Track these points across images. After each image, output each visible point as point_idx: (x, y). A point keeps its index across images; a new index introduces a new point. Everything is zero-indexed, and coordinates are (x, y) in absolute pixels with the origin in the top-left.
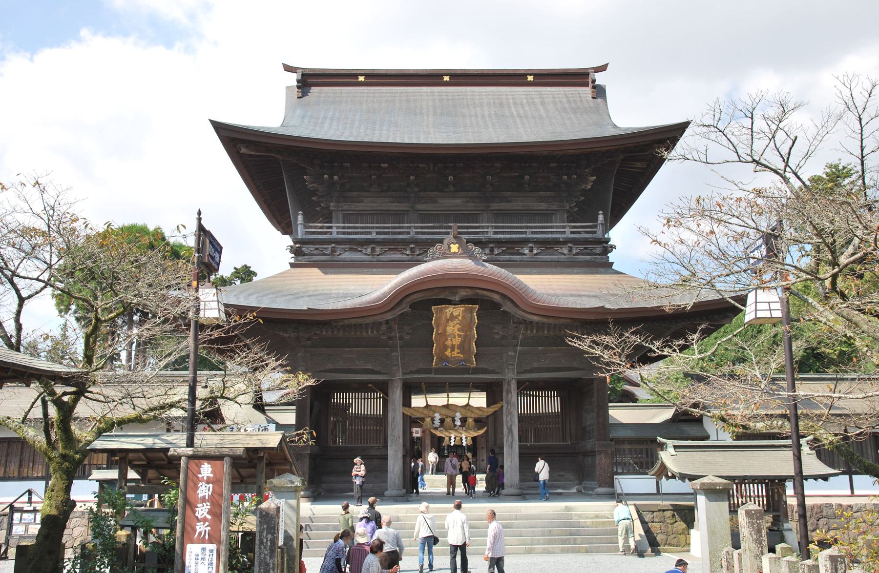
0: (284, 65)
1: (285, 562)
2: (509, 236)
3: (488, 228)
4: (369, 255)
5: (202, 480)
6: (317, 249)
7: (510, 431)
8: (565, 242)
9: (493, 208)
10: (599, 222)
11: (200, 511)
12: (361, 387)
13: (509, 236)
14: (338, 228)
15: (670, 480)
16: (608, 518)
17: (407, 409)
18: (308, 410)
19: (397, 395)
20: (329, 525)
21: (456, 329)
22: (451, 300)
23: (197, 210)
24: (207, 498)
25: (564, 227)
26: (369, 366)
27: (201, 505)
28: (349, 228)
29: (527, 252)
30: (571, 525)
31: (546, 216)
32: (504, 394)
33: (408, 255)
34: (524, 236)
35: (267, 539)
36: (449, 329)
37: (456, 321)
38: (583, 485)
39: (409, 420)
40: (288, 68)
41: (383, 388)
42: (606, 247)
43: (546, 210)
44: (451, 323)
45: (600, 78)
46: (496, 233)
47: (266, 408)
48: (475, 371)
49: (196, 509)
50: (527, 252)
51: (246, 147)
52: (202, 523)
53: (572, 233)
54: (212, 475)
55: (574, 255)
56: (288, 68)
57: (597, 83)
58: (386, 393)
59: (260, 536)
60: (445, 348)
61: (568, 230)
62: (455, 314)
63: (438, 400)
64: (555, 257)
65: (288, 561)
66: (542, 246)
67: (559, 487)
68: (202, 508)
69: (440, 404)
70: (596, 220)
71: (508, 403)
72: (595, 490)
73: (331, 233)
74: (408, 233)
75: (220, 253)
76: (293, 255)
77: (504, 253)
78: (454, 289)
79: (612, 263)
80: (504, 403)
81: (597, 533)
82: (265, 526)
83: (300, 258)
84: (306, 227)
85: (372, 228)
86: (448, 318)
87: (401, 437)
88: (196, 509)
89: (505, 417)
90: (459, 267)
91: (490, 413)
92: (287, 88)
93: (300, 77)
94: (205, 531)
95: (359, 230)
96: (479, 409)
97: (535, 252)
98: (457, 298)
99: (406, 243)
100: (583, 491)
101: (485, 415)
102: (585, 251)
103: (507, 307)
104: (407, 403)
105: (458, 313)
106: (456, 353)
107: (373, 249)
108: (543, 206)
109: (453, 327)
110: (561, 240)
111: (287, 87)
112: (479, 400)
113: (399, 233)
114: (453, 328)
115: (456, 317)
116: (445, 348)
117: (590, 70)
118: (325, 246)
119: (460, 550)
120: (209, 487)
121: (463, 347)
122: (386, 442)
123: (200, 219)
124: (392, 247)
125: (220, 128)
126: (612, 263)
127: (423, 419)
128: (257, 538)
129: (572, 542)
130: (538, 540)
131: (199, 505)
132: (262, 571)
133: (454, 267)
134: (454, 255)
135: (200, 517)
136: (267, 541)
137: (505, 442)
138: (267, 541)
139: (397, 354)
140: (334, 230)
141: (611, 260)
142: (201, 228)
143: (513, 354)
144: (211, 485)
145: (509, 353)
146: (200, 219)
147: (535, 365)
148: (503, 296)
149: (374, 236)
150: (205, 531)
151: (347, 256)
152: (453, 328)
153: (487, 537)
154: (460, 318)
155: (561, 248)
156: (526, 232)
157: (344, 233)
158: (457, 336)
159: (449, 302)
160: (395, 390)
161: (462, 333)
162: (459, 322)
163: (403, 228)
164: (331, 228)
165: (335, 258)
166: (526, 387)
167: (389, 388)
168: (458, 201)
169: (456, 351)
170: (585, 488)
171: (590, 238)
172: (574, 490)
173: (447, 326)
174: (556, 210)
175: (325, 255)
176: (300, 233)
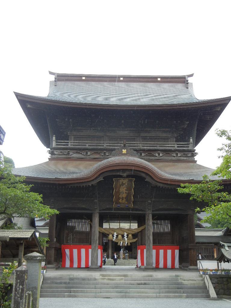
0: (49, 71)
1: (31, 302)
4: (85, 155)
6: (61, 152)
8: (175, 151)
9: (141, 136)
10: (190, 142)
12: (79, 217)
14: (71, 143)
16: (196, 281)
17: (101, 228)
18: (55, 227)
19: (96, 220)
20: (62, 282)
21: (124, 189)
26: (84, 206)
29: (157, 155)
30: (178, 284)
31: (166, 139)
32: (146, 221)
34: (156, 148)
35: (19, 288)
36: (121, 190)
37: (124, 186)
38: (182, 265)
40: (51, 73)
41: (89, 217)
42: (193, 153)
45: (190, 80)
47: (37, 228)
48: (133, 210)
50: (157, 155)
51: (30, 105)
53: (178, 147)
55: (179, 157)
56: (51, 73)
58: (91, 221)
59: (16, 286)
60: (119, 198)
61: (176, 146)
62: (124, 182)
63: (114, 225)
64: (170, 158)
65: (32, 301)
69: (116, 228)
70: (189, 141)
71: (148, 225)
73: (68, 145)
74: (103, 146)
75: (4, 135)
76: (50, 155)
77: (146, 155)
78: (124, 171)
79: (196, 161)
80: (146, 226)
81: (191, 288)
82: (19, 281)
83: (53, 156)
84: (56, 142)
85: (87, 143)
86: (121, 184)
87: (98, 240)
89: (146, 231)
92: (50, 82)
93: (56, 77)
96: (135, 229)
98: (125, 175)
99: (102, 150)
100: (182, 268)
101: (136, 231)
102: (183, 155)
103: (148, 179)
104: (101, 225)
107: (87, 153)
108: (164, 135)
115: (124, 184)
116: (119, 198)
118: (65, 151)
119: (2, 273)
121: (128, 198)
126: (196, 161)
127: (108, 235)
128: (14, 288)
129: (179, 292)
132: (16, 306)
134: (124, 154)
138: (19, 290)
140: (70, 143)
141: (196, 160)
145: (149, 201)
147: (161, 207)
149: (87, 147)
154: (126, 184)
157: (74, 145)
159: (121, 176)
160: (95, 218)
164: (68, 143)
165: (69, 156)
166: (157, 218)
167: (93, 216)
168: (126, 132)
169: (124, 200)
170: (183, 266)
173: (120, 188)
175: (65, 155)
176: (54, 144)
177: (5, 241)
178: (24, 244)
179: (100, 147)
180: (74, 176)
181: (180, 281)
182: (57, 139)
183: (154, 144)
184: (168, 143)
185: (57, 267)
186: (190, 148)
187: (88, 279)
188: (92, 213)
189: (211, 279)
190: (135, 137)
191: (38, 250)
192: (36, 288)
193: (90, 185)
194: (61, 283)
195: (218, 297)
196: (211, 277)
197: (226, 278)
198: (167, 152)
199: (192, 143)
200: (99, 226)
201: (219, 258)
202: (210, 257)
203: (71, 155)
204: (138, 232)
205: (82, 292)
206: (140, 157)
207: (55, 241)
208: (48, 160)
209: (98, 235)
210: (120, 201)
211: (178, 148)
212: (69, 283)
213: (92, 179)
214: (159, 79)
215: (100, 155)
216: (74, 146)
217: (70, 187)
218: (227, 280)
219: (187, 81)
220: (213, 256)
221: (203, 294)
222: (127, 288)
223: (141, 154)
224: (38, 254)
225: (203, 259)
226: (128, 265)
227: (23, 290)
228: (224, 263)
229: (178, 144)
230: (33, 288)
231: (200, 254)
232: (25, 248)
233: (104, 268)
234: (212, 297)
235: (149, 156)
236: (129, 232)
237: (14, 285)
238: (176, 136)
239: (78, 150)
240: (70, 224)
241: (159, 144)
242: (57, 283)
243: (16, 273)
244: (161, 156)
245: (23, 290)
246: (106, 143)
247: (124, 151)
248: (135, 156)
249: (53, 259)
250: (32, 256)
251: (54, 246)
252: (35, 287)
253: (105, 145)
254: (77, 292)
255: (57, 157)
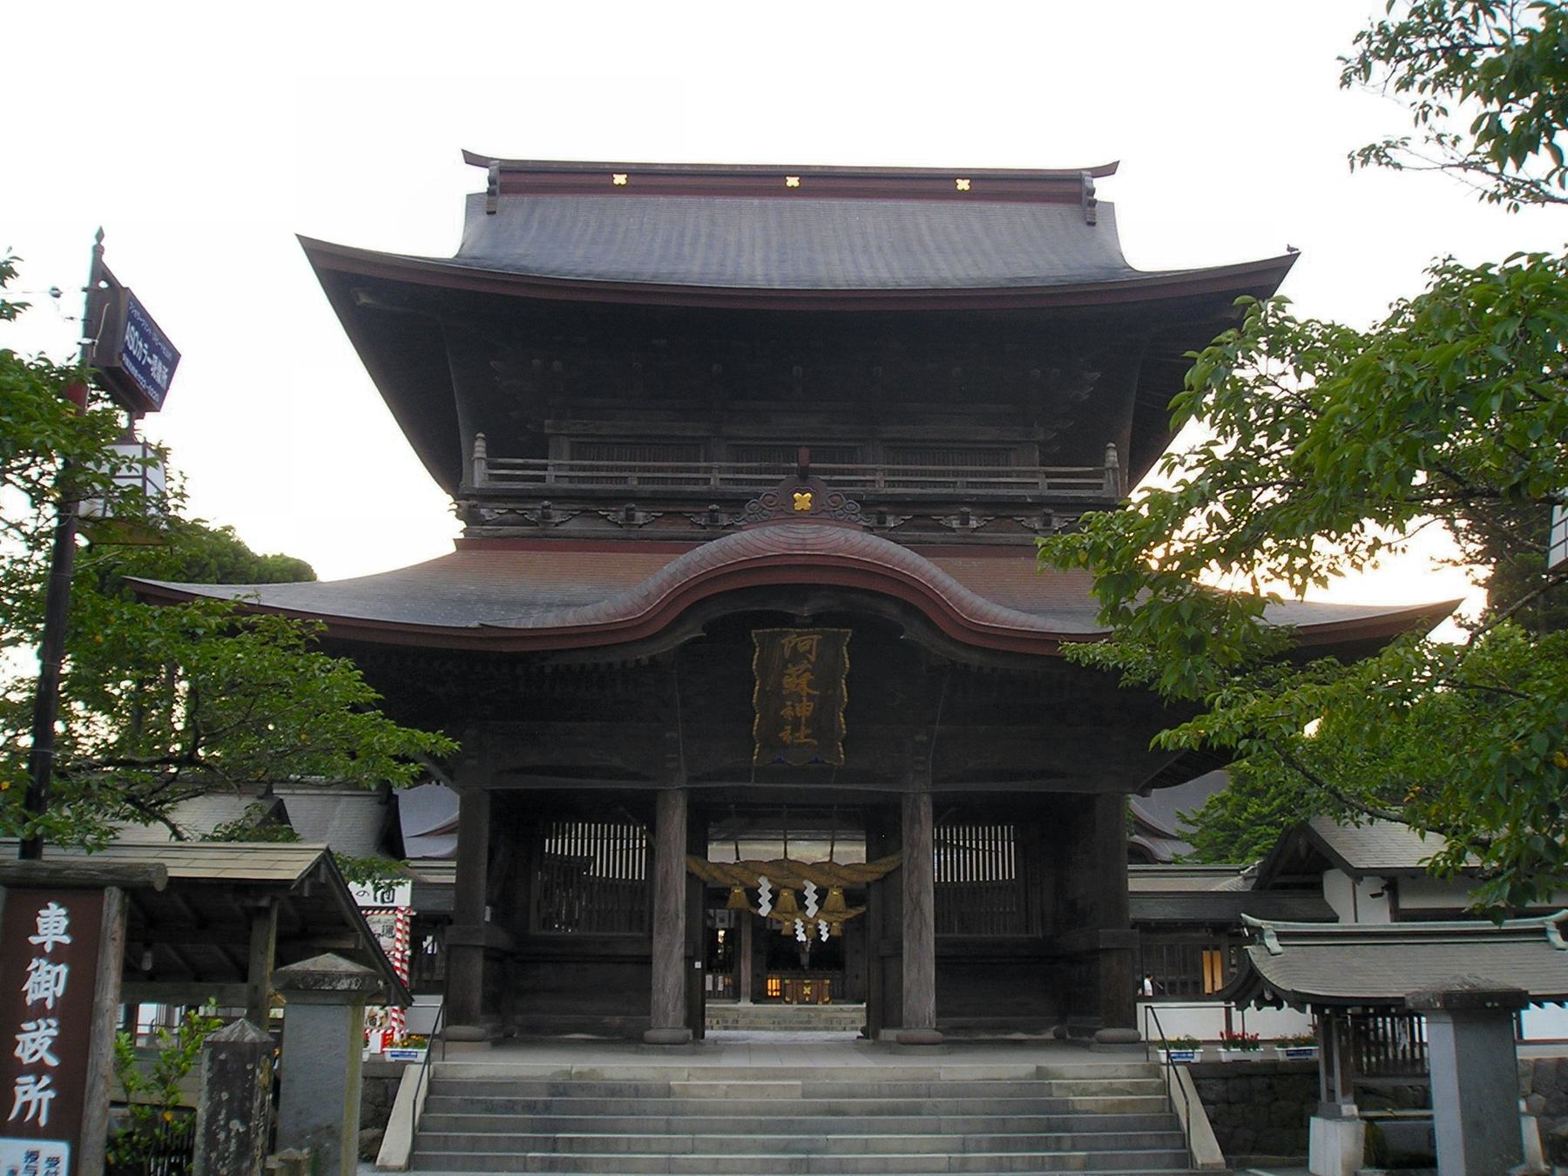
2: (918, 491)
3: (875, 475)
4: (621, 526)
5: (39, 951)
6: (512, 511)
7: (917, 904)
8: (1039, 504)
9: (885, 436)
10: (1108, 465)
11: (29, 1044)
13: (918, 491)
15: (1266, 1009)
20: (515, 1102)
21: (803, 682)
22: (793, 616)
23: (96, 230)
24: (49, 1004)
25: (1033, 474)
27: (31, 1026)
28: (584, 468)
29: (955, 524)
30: (1051, 1107)
33: (704, 527)
34: (951, 491)
35: (229, 1131)
37: (805, 665)
39: (701, 890)
40: (472, 159)
43: (993, 442)
44: (792, 670)
45: (1103, 189)
46: (892, 484)
49: (19, 1037)
50: (955, 524)
52: (31, 1079)
53: (1051, 486)
54: (66, 940)
56: (472, 159)
57: (1095, 197)
58: (652, 830)
59: (208, 1129)
61: (1043, 482)
66: (988, 512)
67: (1016, 1029)
68: (33, 1035)
72: (1098, 1033)
73: (542, 479)
74: (707, 481)
76: (462, 525)
78: (799, 592)
81: (1106, 1126)
82: (225, 1096)
83: (477, 529)
84: (491, 466)
86: (787, 657)
87: (682, 915)
88: (19, 1037)
90: (809, 542)
91: (869, 878)
94: (40, 1101)
95: (603, 474)
97: (973, 524)
98: (806, 611)
100: (1068, 1037)
103: (912, 632)
104: (697, 847)
105: (808, 647)
106: (802, 737)
109: (798, 677)
110: (1029, 500)
111: (469, 196)
112: (853, 852)
113: (688, 481)
114: (797, 681)
117: (1084, 172)
120: (58, 974)
122: (651, 930)
123: (98, 251)
124: (670, 509)
125: (297, 235)
129: (560, 1143)
130: (979, 1141)
131: (25, 1026)
133: (801, 542)
134: (802, 517)
135: (26, 1061)
136: (228, 1138)
137: (905, 929)
138: (228, 1138)
139: (675, 735)
140: (550, 474)
142: (100, 271)
143: (925, 738)
144: (63, 969)
145: (918, 738)
146: (98, 251)
148: (909, 609)
149: (633, 484)
150: (40, 1101)
151: (575, 526)
152: (797, 681)
153: (754, 1001)
154: (812, 658)
155: (1028, 517)
156: (956, 482)
158: (804, 699)
159: (787, 621)
161: (815, 693)
162: (810, 667)
163: (697, 470)
164: (545, 468)
165: (552, 531)
169: (804, 731)
171: (1090, 498)
172: (1049, 1035)
174: (1016, 442)
177: (149, 888)
178: (280, 918)
179: (690, 488)
180: (571, 618)
181: (1058, 1095)
182: (494, 450)
183: (943, 474)
184: (1008, 469)
185: (501, 1035)
186: (1105, 493)
187: (637, 1089)
188: (655, 793)
189: (1198, 1088)
190: (857, 444)
191: (356, 946)
192: (332, 1132)
193: (645, 661)
194: (510, 1107)
195: (1228, 1163)
196: (1200, 1075)
197: (1265, 1076)
198: (1002, 509)
199: (1114, 470)
200: (690, 852)
201: (1237, 991)
202: (1188, 989)
203: (557, 525)
204: (868, 885)
205: (606, 1146)
206: (878, 528)
207: (487, 919)
208: (452, 549)
209: (682, 896)
210: (786, 735)
211: (1055, 493)
212: (548, 1107)
213: (649, 632)
214: (963, 185)
215: (693, 523)
216: (570, 482)
217: (548, 670)
218: (1270, 1087)
219: (1092, 192)
220: (1199, 984)
221: (1164, 1151)
222: (817, 1132)
223: (882, 521)
224: (345, 965)
225: (1159, 995)
226: (827, 1029)
227: (245, 1142)
228: (1259, 1009)
229: (1049, 475)
230: (317, 1130)
231: (1148, 976)
232: (281, 940)
233: (715, 1041)
234: (1203, 1165)
235: (918, 528)
236: (824, 881)
237: (201, 1112)
238: (1041, 437)
239: (588, 502)
240: (555, 846)
241: (964, 473)
242: (490, 1107)
243: (213, 1058)
244: (975, 530)
245: (245, 1142)
246: (720, 470)
247: (803, 500)
248: (851, 524)
249: (476, 998)
250: (311, 973)
251: (482, 944)
252: (329, 1127)
253: (717, 476)
254: (585, 1145)
255: (491, 533)
